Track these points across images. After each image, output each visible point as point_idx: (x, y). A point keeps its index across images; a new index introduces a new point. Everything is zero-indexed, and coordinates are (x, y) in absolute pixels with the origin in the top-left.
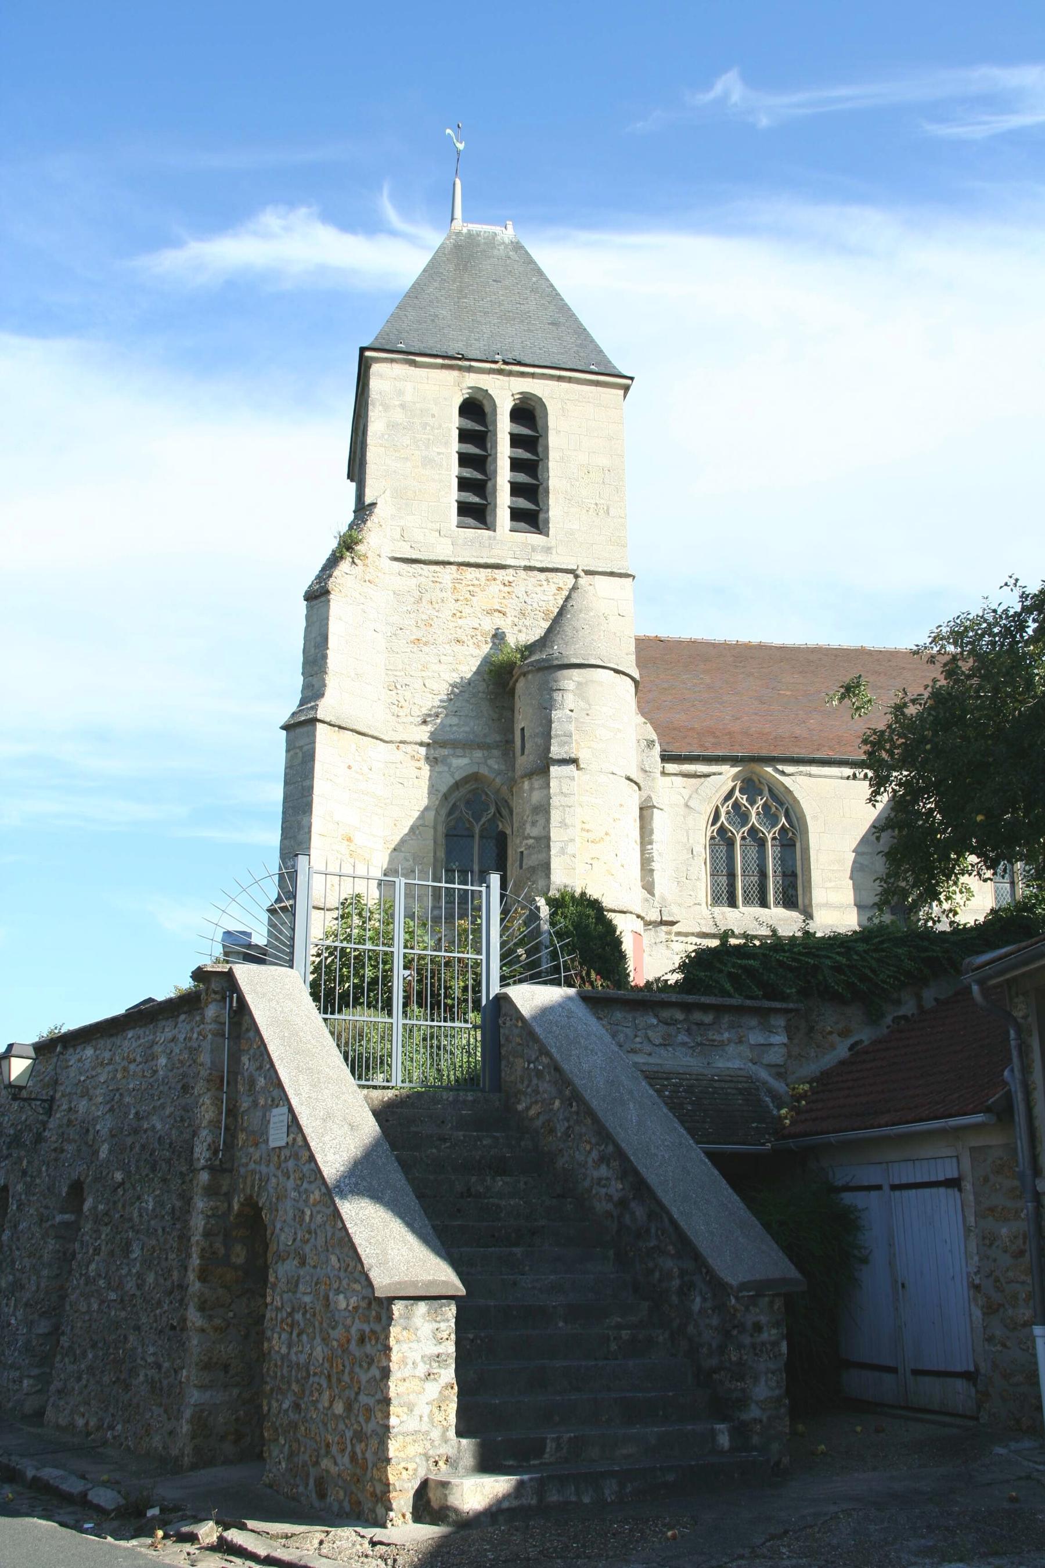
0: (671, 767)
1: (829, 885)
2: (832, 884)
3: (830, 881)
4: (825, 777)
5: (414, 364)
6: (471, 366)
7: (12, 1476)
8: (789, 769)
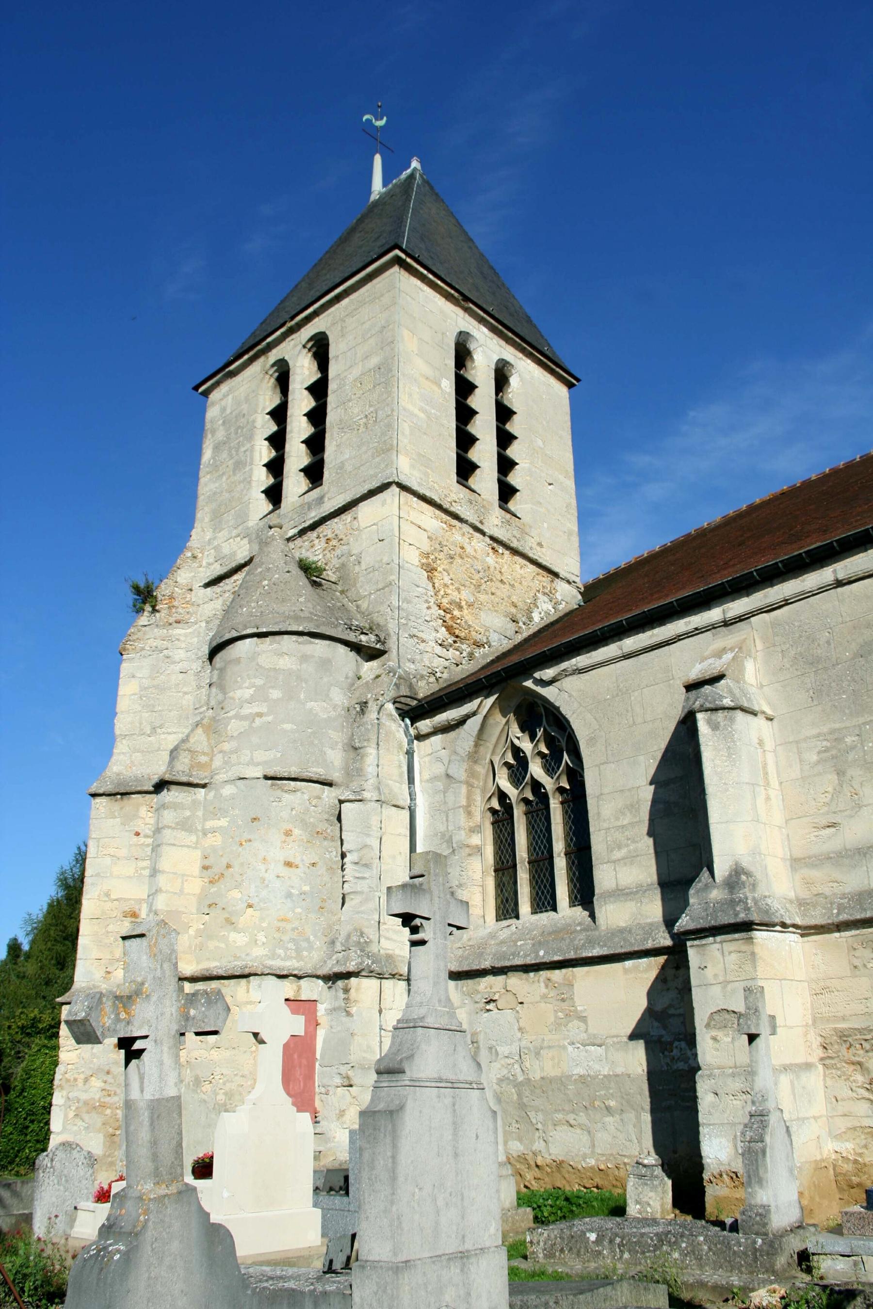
0: (425, 725)
1: (618, 854)
2: (624, 852)
3: (620, 847)
4: (697, 631)
5: (233, 374)
6: (268, 344)
7: (868, 626)
8: (548, 673)
